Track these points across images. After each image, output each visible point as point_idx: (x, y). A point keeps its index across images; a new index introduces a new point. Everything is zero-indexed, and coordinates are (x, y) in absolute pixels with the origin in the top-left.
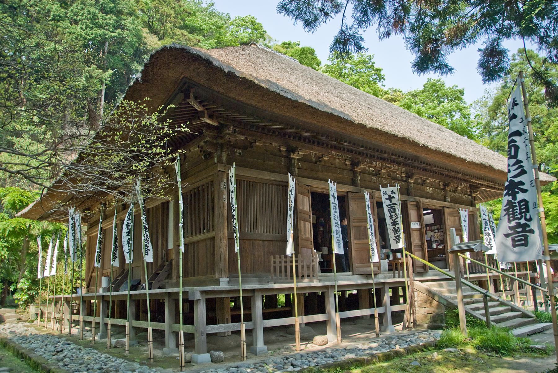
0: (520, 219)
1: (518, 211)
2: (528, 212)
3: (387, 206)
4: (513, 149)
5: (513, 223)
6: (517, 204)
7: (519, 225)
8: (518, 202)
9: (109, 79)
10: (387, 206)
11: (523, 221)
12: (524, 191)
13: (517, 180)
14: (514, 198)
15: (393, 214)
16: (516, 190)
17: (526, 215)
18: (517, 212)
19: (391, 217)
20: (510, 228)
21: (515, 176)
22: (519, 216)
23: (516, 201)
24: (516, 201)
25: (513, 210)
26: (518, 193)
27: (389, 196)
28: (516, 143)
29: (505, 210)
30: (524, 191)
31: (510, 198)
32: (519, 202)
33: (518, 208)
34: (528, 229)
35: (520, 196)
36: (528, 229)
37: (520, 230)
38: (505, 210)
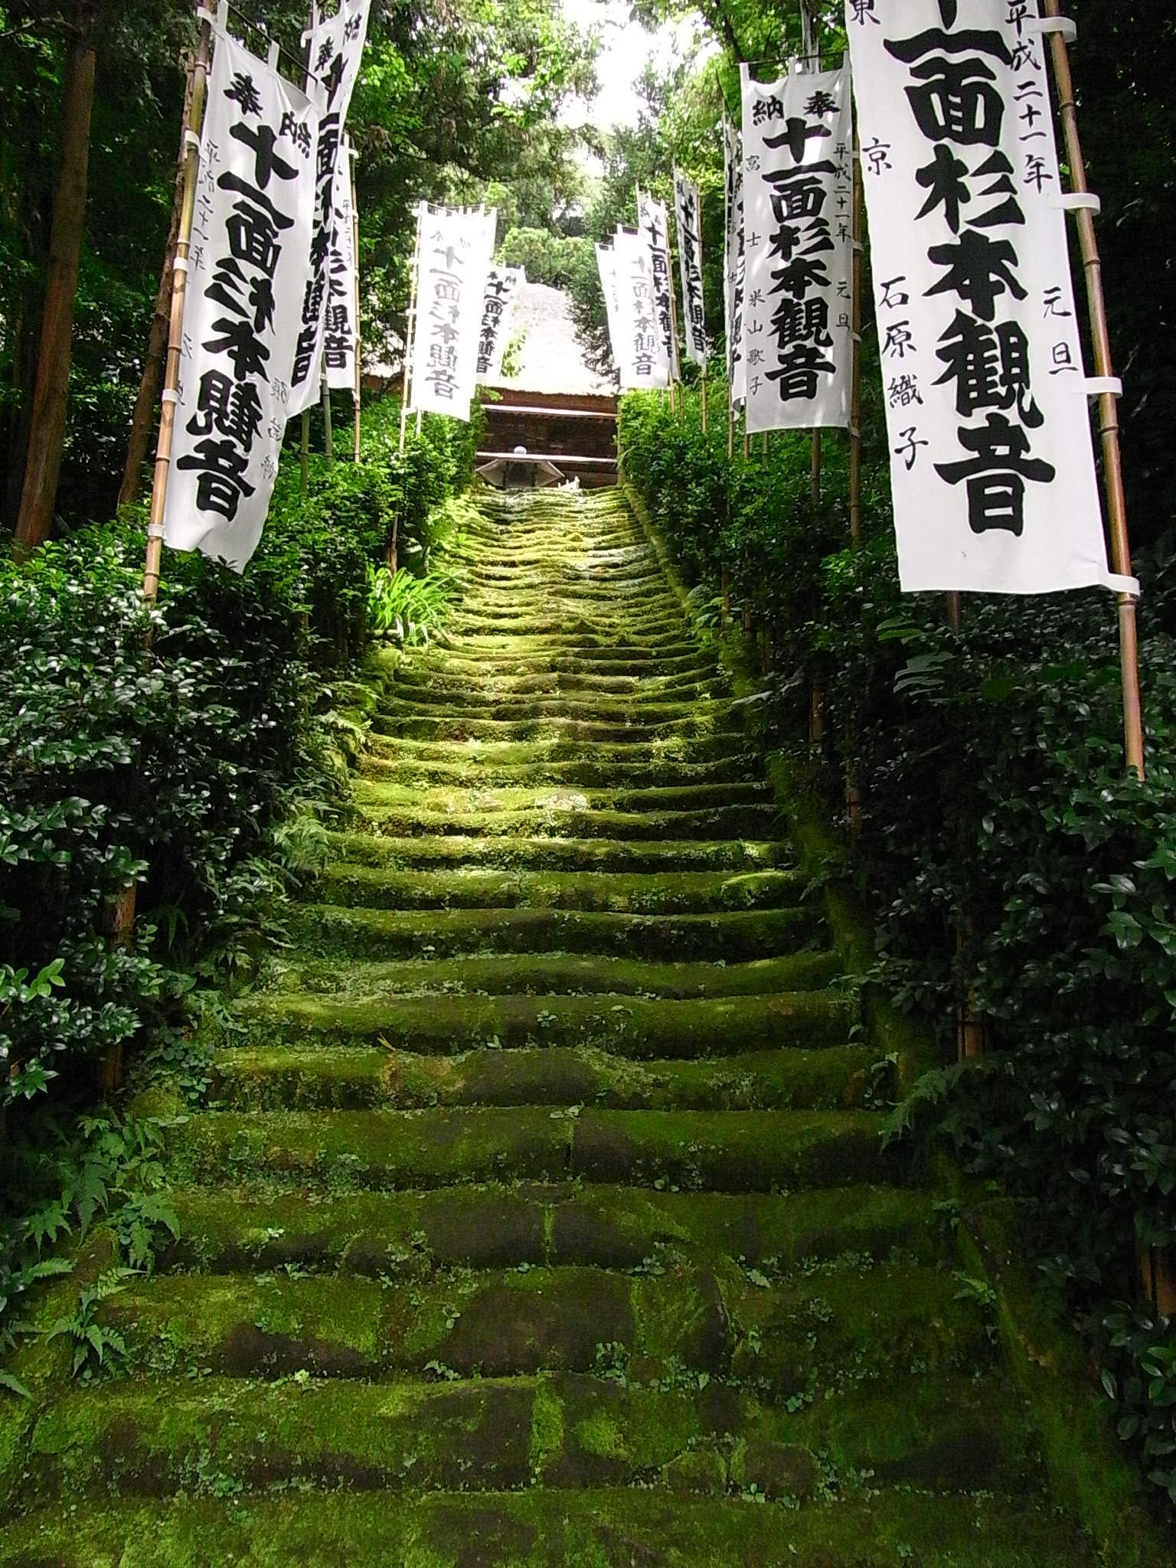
0: (806, 337)
1: (803, 321)
2: (825, 327)
3: (901, 50)
4: (812, 196)
5: (978, 419)
6: (995, 337)
7: (800, 351)
8: (997, 329)
9: (145, 57)
10: (901, 50)
11: (809, 343)
12: (824, 282)
13: (994, 233)
14: (800, 294)
15: (972, 155)
16: (993, 277)
17: (819, 332)
18: (994, 371)
19: (943, 182)
20: (966, 437)
21: (805, 253)
22: (804, 332)
23: (802, 302)
24: (992, 325)
25: (794, 319)
26: (810, 283)
27: (791, 122)
28: (990, 82)
29: (942, 354)
30: (824, 282)
31: (790, 295)
32: (809, 304)
33: (997, 352)
34: (819, 360)
35: (812, 291)
36: (819, 360)
37: (802, 360)
38: (942, 354)
